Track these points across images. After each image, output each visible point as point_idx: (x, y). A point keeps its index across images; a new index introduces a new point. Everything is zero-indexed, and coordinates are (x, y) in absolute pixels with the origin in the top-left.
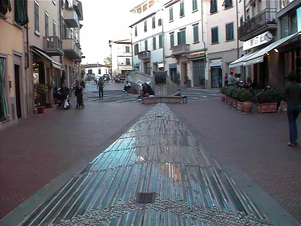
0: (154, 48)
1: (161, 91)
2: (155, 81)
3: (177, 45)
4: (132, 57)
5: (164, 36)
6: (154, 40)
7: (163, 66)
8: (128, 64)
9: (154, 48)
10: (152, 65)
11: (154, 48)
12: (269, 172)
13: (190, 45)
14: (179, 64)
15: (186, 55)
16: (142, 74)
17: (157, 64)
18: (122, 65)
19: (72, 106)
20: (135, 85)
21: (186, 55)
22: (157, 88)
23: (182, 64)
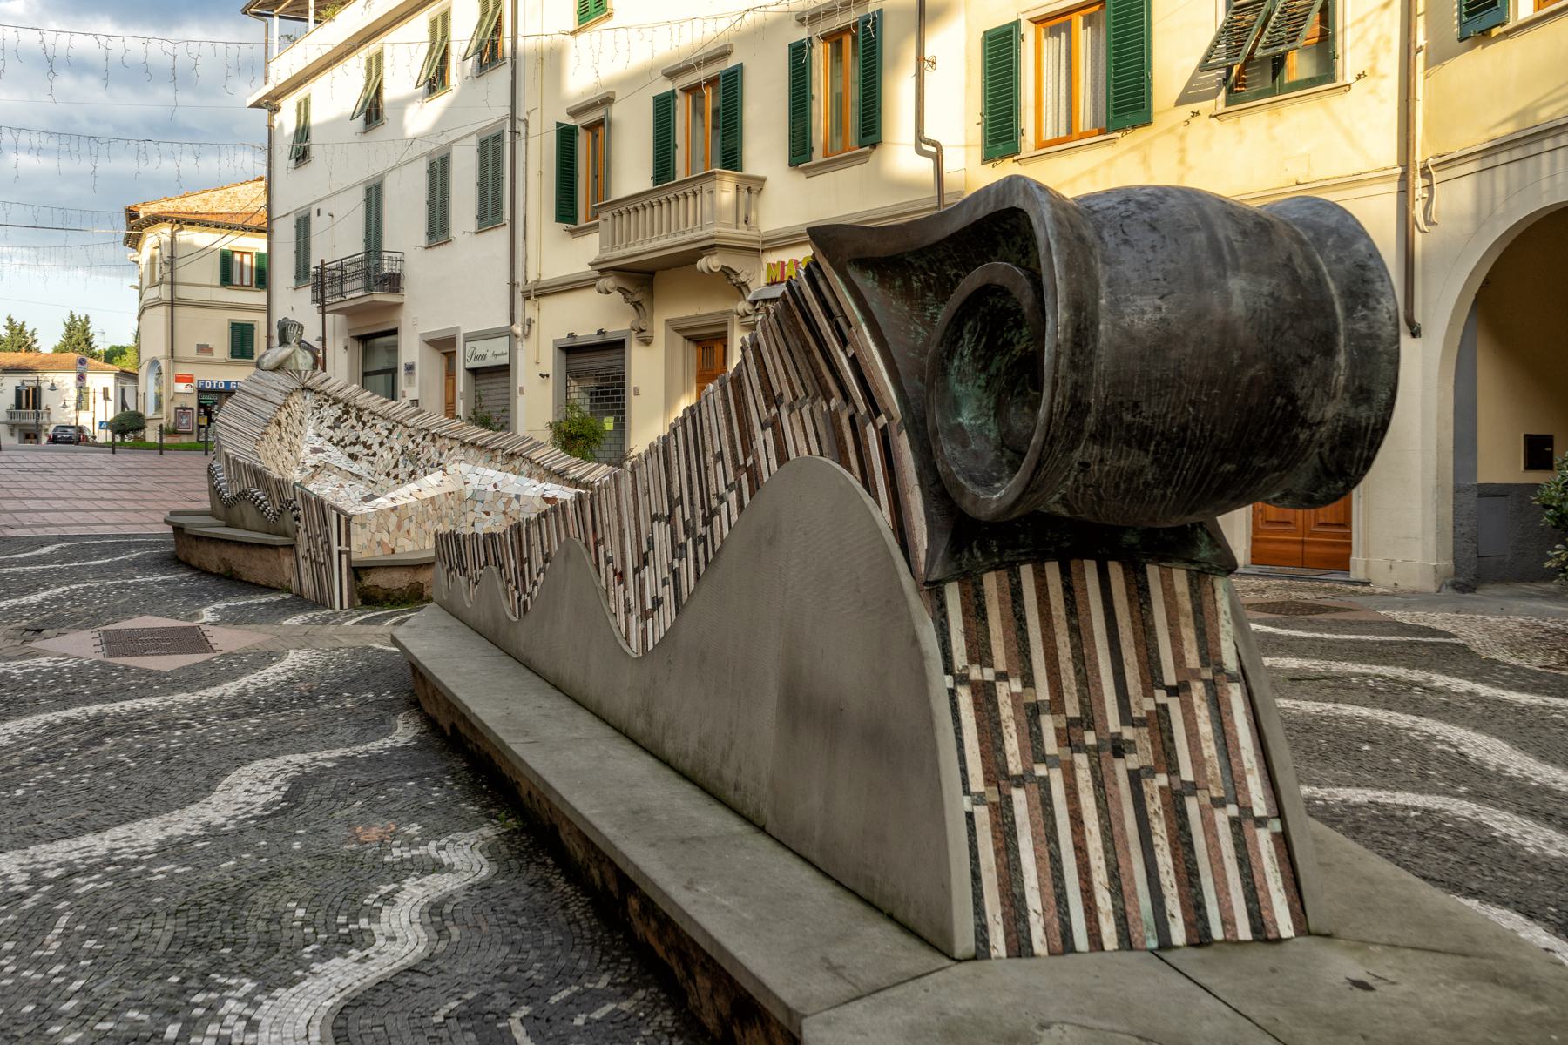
0: (431, 234)
1: (1121, 768)
2: (1479, 594)
3: (648, 185)
4: (269, 238)
5: (520, 145)
6: (439, 170)
7: (504, 360)
8: (243, 356)
9: (438, 230)
10: (417, 350)
11: (438, 230)
12: (372, 497)
13: (767, 185)
14: (647, 342)
15: (734, 262)
16: (519, 279)
17: (452, 341)
18: (204, 356)
19: (1225, 131)
20: (287, 505)
21: (734, 262)
22: (985, 695)
23: (679, 338)
